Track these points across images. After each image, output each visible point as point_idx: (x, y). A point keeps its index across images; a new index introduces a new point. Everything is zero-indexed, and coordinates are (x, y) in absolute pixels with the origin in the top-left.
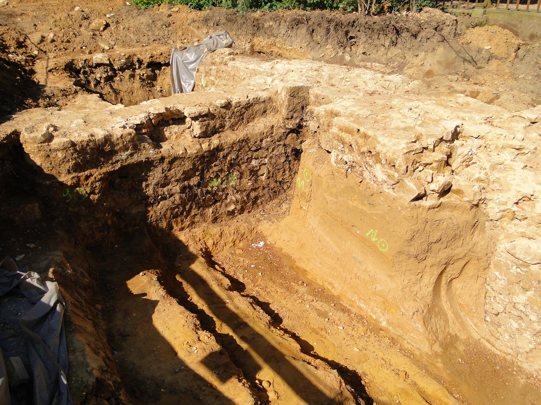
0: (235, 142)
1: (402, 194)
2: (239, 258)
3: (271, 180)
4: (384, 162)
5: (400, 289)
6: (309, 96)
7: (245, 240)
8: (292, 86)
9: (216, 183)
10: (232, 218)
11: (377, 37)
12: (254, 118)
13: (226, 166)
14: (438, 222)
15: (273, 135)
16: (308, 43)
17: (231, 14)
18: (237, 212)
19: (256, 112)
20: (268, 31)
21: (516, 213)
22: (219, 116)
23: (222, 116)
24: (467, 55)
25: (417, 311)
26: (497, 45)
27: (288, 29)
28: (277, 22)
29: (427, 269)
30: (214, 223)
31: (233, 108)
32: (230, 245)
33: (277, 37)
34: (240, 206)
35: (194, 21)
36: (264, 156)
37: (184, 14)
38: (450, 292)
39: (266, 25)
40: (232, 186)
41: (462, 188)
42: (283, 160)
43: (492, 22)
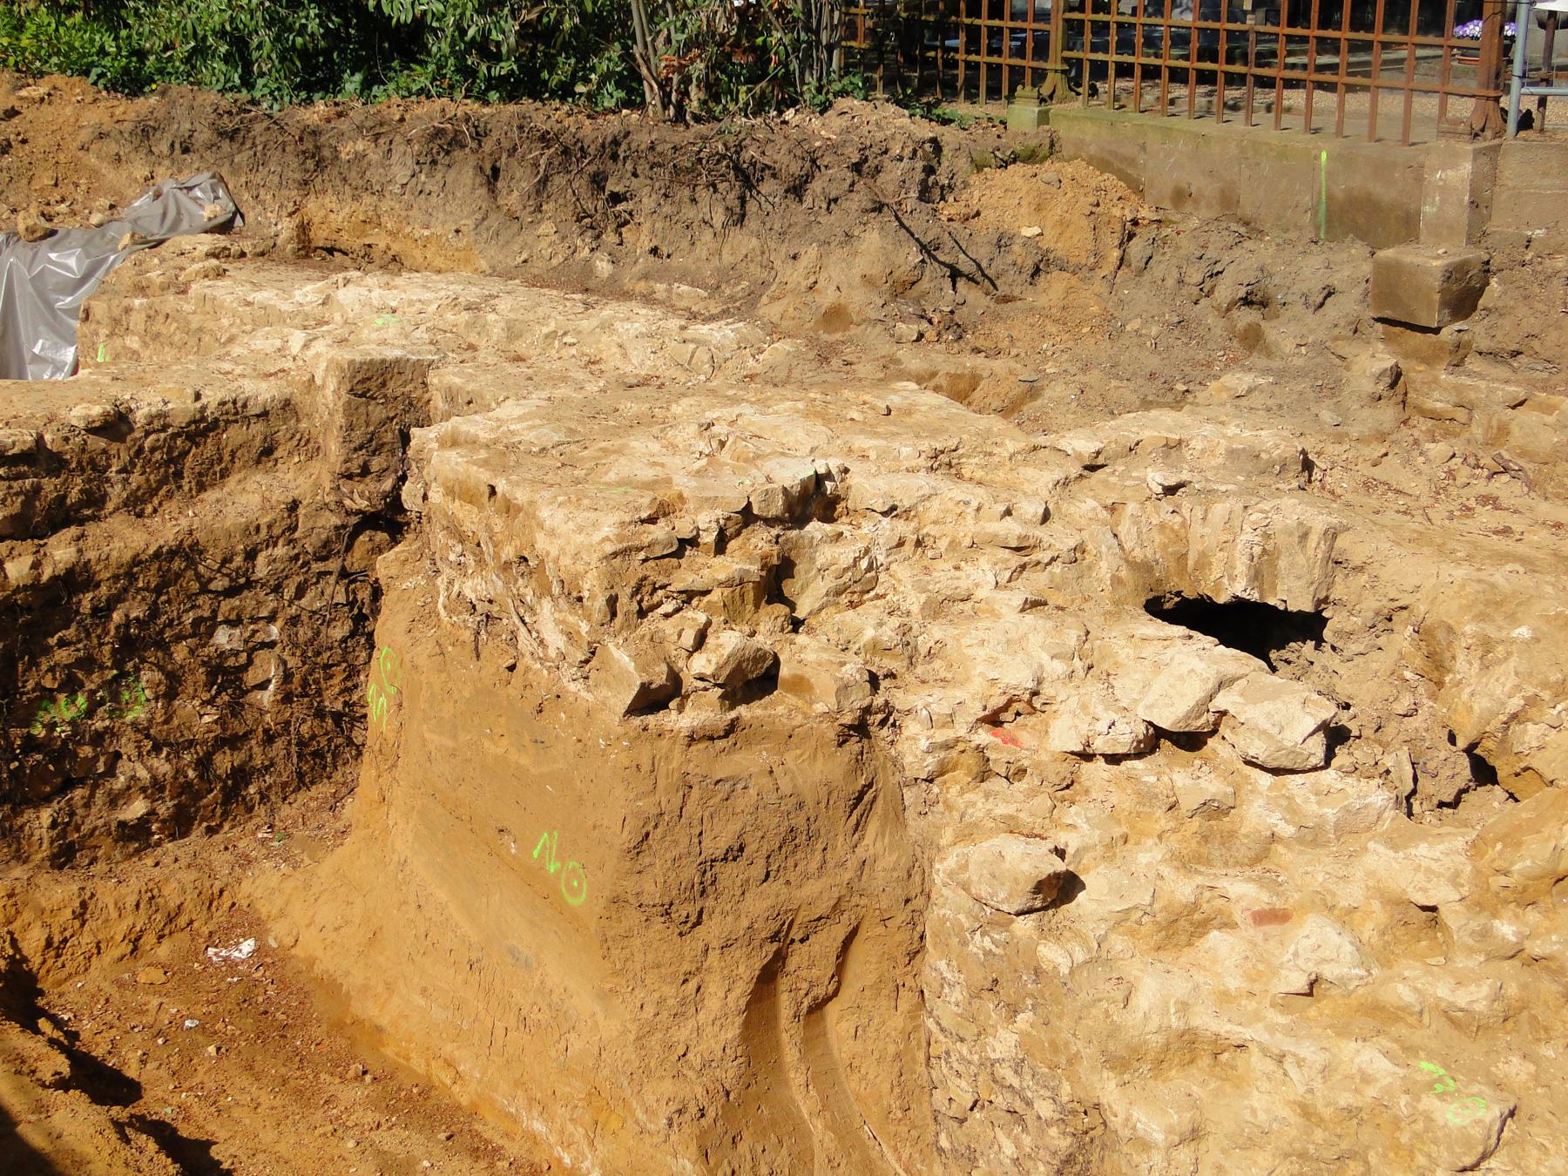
0: (143, 557)
1: (605, 692)
2: (146, 998)
3: (299, 709)
4: (556, 590)
5: (632, 1037)
6: (426, 396)
7: (184, 936)
8: (358, 358)
9: (65, 711)
10: (137, 851)
11: (687, 192)
12: (224, 474)
13: (107, 649)
14: (727, 786)
15: (297, 535)
16: (479, 216)
17: (230, 113)
18: (161, 830)
19: (233, 454)
20: (354, 173)
21: (988, 753)
22: (79, 463)
23: (92, 461)
24: (962, 256)
25: (680, 1112)
26: (1063, 224)
27: (417, 168)
28: (381, 141)
29: (714, 956)
30: (61, 868)
31: (137, 434)
32: (117, 953)
33: (381, 193)
34: (170, 804)
35: (101, 136)
36: (264, 613)
37: (69, 111)
38: (819, 1052)
39: (347, 150)
40: (134, 725)
41: (808, 672)
42: (339, 631)
43: (1067, 150)
